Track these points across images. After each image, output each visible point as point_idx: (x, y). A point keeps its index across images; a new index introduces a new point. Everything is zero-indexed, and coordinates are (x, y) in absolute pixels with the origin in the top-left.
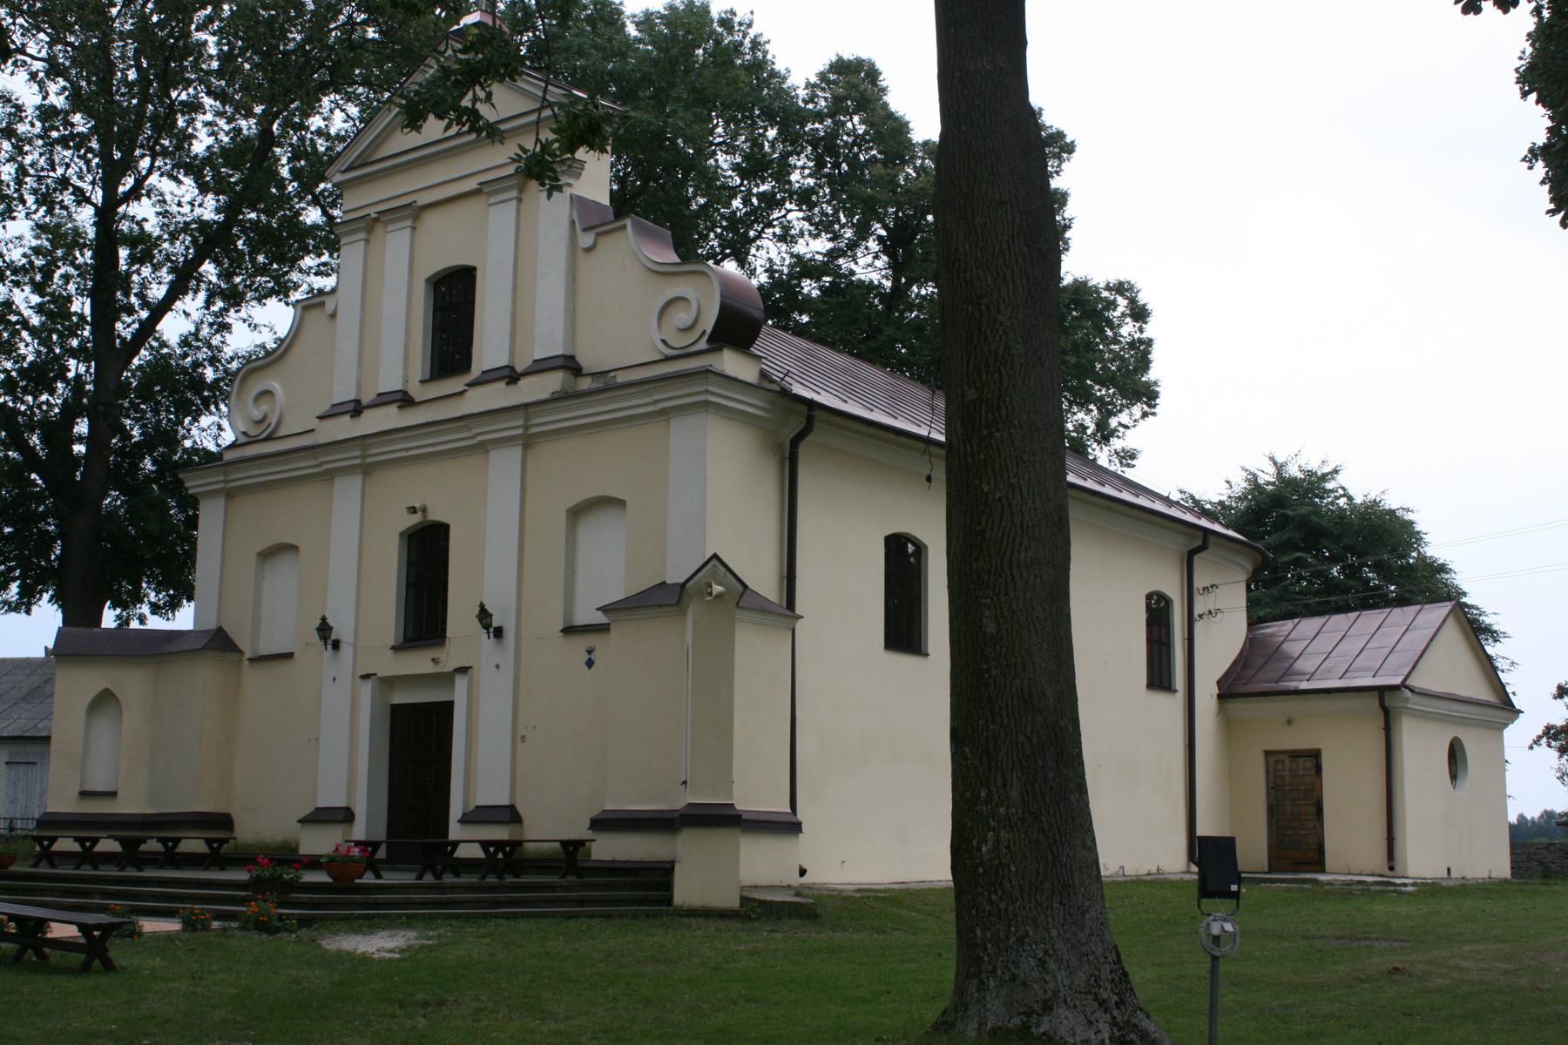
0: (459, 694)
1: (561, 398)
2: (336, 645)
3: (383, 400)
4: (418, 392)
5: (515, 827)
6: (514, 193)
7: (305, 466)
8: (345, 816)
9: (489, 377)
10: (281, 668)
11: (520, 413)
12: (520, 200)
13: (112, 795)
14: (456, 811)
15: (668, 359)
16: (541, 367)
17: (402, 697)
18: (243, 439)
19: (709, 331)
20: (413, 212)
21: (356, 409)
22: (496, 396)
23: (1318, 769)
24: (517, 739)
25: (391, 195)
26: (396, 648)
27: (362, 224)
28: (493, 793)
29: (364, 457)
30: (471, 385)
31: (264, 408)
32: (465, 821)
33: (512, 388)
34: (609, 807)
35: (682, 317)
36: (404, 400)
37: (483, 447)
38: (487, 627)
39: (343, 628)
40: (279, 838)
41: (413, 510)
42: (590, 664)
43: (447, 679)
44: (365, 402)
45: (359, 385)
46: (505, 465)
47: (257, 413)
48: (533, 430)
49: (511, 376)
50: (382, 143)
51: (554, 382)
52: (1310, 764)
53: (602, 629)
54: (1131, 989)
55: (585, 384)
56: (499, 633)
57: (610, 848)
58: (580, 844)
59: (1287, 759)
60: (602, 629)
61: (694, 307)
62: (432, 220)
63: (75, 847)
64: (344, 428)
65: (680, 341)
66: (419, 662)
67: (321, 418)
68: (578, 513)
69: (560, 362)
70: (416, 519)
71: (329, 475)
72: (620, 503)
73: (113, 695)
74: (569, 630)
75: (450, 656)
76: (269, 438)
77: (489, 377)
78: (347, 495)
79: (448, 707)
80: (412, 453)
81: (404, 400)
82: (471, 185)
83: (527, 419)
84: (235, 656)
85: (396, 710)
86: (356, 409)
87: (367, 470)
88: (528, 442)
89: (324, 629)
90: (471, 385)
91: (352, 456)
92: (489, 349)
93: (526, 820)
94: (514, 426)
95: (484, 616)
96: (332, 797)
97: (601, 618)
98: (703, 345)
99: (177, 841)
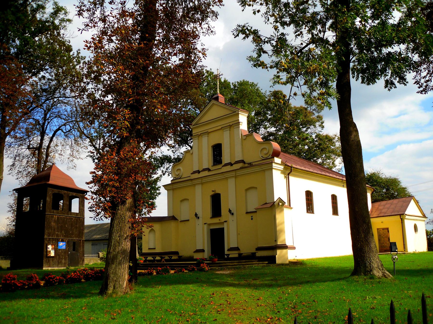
0: (225, 226)
1: (241, 168)
2: (198, 218)
3: (204, 170)
4: (211, 168)
5: (239, 251)
6: (229, 129)
7: (189, 183)
8: (203, 251)
9: (226, 165)
10: (186, 222)
11: (234, 172)
12: (230, 130)
13: (155, 249)
14: (226, 248)
15: (263, 160)
16: (237, 162)
17: (212, 227)
18: (175, 179)
19: (271, 154)
20: (208, 133)
21: (199, 172)
22: (228, 168)
23: (388, 231)
24: (238, 234)
25: (234, 120)
26: (211, 218)
27: (197, 136)
28: (234, 245)
29: (202, 181)
30: (223, 166)
31: (179, 172)
32: (228, 250)
33: (232, 167)
34: (259, 246)
35: (265, 152)
36: (209, 170)
37: (227, 178)
38: (230, 213)
39: (200, 215)
40: (189, 256)
41: (213, 191)
42: (252, 219)
43: (222, 223)
44: (200, 171)
45: (231, 159)
46: (231, 183)
47: (177, 173)
48: (237, 175)
49: (231, 164)
50: (200, 120)
51: (241, 165)
52: (386, 231)
53: (256, 212)
54: (240, 278)
55: (246, 165)
56: (233, 214)
57: (260, 254)
58: (255, 253)
59: (382, 230)
60: (256, 212)
61: (268, 150)
62: (211, 135)
63: (168, 258)
64: (196, 176)
65: (265, 156)
66: (216, 220)
67: (191, 174)
68: (247, 190)
69: (241, 161)
70: (213, 193)
71: (194, 185)
72: (256, 188)
73: (154, 230)
74: (247, 213)
75: (223, 219)
76: (180, 178)
77: (226, 165)
78: (198, 189)
79: (223, 229)
80: (256, 171)
81: (209, 170)
82: (220, 127)
83: (236, 172)
84: (177, 221)
85: (211, 230)
86: (199, 172)
87: (236, 177)
88: (236, 177)
89: (196, 215)
90: (223, 166)
91: (199, 181)
92: (226, 159)
93: (241, 250)
94: (233, 174)
95: (230, 211)
96: (200, 247)
97: (255, 210)
98: (270, 157)
99: (172, 257)
